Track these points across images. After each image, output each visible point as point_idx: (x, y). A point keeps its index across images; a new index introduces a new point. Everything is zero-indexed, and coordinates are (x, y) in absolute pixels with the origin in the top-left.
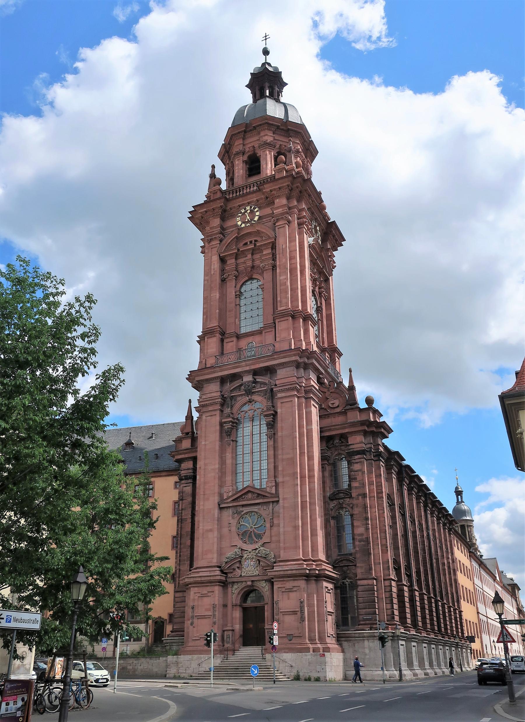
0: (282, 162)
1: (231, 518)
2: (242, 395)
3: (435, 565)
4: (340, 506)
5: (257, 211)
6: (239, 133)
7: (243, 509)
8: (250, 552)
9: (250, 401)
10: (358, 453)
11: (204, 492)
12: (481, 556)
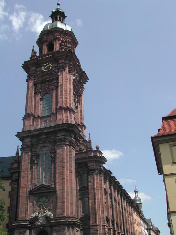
0: (63, 45)
3: (125, 220)
12: (145, 219)
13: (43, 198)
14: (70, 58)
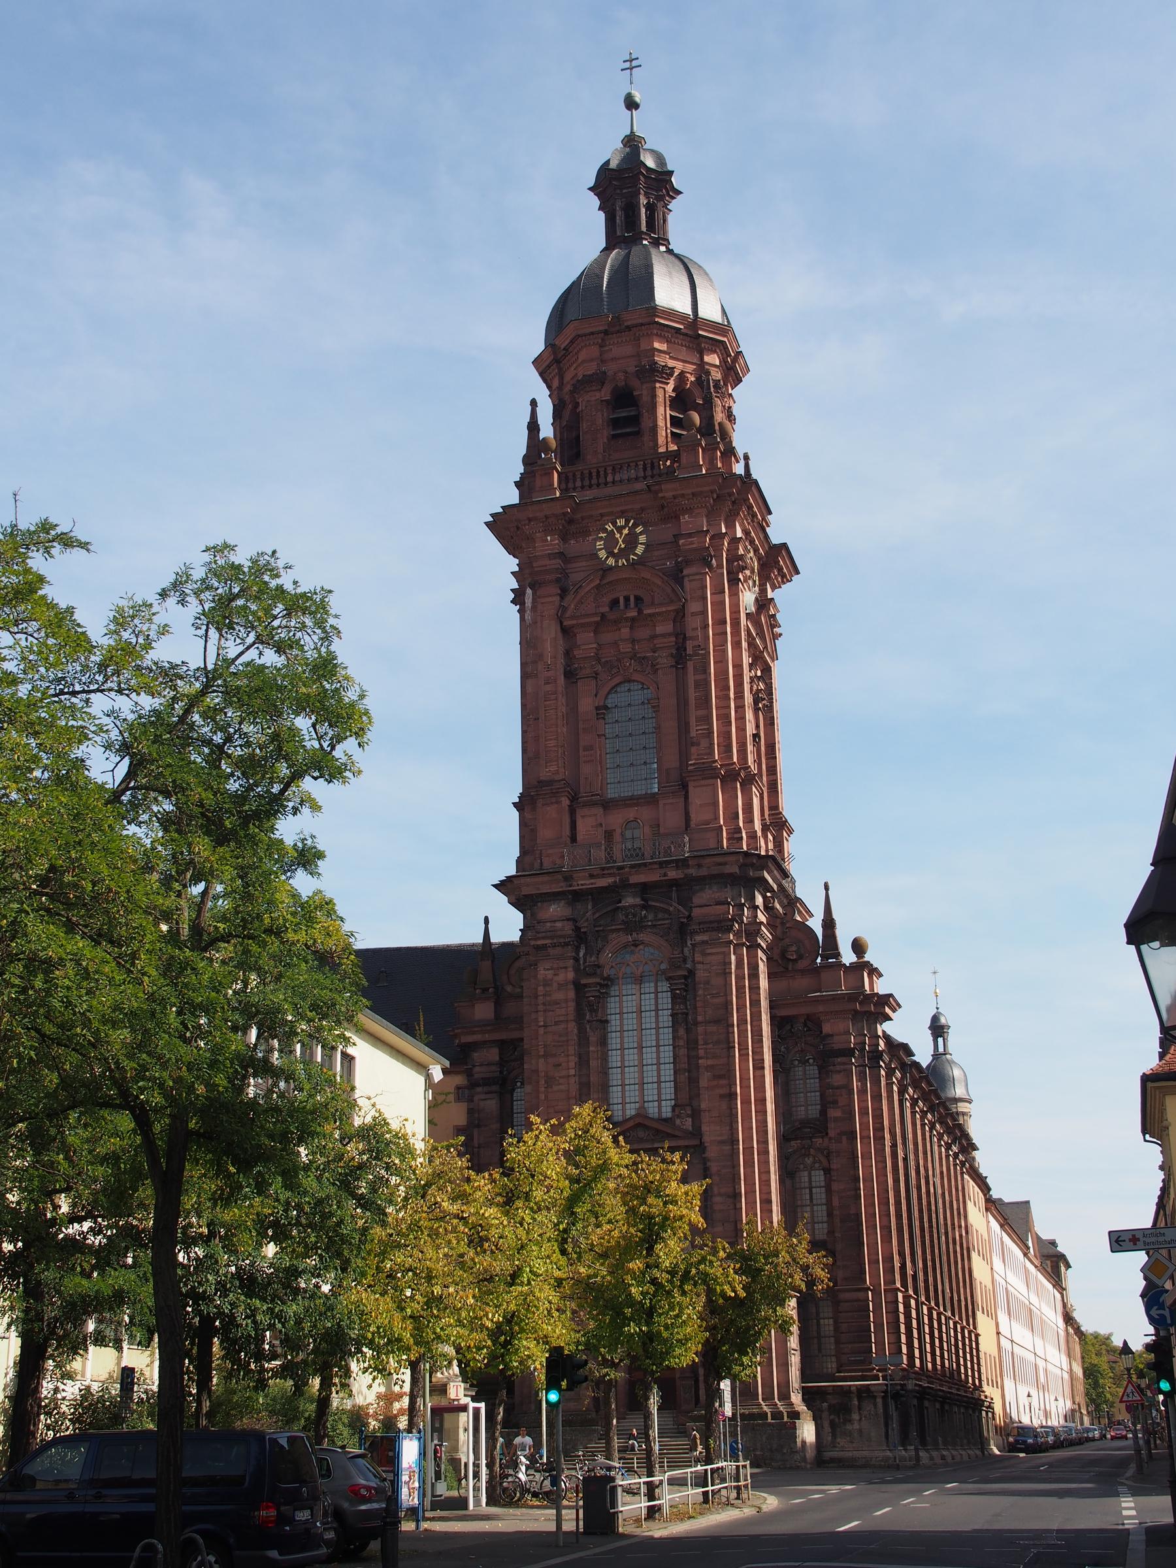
2: (618, 930)
5: (641, 533)
14: (734, 503)
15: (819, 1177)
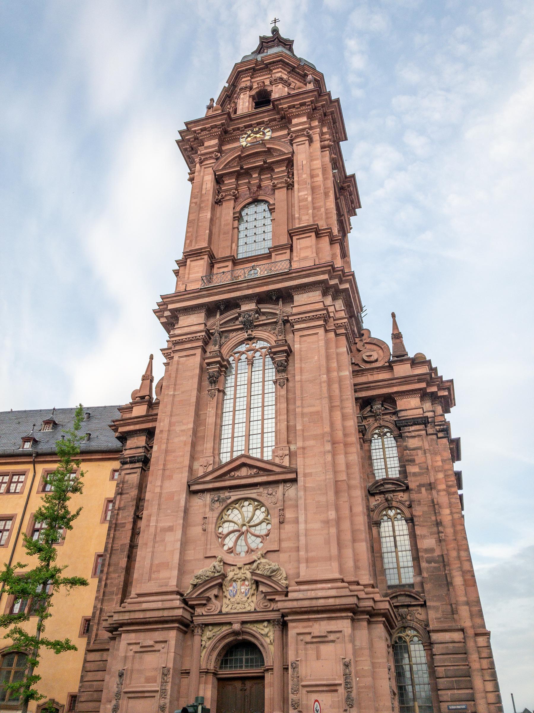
1: (207, 509)
4: (386, 505)
6: (247, 70)
7: (231, 494)
8: (240, 568)
9: (250, 339)
10: (415, 421)
11: (164, 465)
13: (244, 509)
15: (402, 527)
